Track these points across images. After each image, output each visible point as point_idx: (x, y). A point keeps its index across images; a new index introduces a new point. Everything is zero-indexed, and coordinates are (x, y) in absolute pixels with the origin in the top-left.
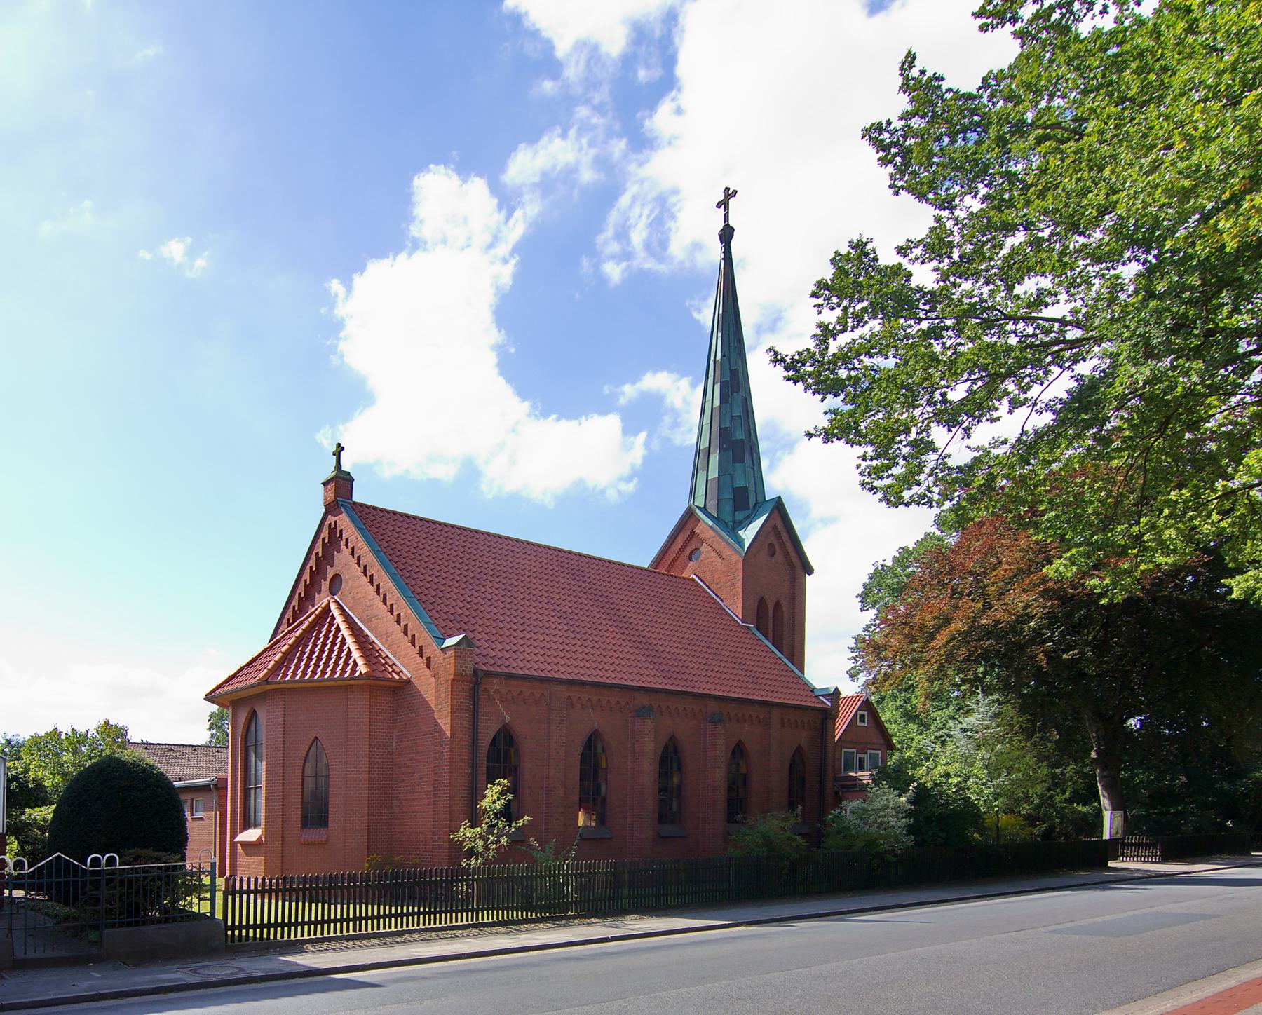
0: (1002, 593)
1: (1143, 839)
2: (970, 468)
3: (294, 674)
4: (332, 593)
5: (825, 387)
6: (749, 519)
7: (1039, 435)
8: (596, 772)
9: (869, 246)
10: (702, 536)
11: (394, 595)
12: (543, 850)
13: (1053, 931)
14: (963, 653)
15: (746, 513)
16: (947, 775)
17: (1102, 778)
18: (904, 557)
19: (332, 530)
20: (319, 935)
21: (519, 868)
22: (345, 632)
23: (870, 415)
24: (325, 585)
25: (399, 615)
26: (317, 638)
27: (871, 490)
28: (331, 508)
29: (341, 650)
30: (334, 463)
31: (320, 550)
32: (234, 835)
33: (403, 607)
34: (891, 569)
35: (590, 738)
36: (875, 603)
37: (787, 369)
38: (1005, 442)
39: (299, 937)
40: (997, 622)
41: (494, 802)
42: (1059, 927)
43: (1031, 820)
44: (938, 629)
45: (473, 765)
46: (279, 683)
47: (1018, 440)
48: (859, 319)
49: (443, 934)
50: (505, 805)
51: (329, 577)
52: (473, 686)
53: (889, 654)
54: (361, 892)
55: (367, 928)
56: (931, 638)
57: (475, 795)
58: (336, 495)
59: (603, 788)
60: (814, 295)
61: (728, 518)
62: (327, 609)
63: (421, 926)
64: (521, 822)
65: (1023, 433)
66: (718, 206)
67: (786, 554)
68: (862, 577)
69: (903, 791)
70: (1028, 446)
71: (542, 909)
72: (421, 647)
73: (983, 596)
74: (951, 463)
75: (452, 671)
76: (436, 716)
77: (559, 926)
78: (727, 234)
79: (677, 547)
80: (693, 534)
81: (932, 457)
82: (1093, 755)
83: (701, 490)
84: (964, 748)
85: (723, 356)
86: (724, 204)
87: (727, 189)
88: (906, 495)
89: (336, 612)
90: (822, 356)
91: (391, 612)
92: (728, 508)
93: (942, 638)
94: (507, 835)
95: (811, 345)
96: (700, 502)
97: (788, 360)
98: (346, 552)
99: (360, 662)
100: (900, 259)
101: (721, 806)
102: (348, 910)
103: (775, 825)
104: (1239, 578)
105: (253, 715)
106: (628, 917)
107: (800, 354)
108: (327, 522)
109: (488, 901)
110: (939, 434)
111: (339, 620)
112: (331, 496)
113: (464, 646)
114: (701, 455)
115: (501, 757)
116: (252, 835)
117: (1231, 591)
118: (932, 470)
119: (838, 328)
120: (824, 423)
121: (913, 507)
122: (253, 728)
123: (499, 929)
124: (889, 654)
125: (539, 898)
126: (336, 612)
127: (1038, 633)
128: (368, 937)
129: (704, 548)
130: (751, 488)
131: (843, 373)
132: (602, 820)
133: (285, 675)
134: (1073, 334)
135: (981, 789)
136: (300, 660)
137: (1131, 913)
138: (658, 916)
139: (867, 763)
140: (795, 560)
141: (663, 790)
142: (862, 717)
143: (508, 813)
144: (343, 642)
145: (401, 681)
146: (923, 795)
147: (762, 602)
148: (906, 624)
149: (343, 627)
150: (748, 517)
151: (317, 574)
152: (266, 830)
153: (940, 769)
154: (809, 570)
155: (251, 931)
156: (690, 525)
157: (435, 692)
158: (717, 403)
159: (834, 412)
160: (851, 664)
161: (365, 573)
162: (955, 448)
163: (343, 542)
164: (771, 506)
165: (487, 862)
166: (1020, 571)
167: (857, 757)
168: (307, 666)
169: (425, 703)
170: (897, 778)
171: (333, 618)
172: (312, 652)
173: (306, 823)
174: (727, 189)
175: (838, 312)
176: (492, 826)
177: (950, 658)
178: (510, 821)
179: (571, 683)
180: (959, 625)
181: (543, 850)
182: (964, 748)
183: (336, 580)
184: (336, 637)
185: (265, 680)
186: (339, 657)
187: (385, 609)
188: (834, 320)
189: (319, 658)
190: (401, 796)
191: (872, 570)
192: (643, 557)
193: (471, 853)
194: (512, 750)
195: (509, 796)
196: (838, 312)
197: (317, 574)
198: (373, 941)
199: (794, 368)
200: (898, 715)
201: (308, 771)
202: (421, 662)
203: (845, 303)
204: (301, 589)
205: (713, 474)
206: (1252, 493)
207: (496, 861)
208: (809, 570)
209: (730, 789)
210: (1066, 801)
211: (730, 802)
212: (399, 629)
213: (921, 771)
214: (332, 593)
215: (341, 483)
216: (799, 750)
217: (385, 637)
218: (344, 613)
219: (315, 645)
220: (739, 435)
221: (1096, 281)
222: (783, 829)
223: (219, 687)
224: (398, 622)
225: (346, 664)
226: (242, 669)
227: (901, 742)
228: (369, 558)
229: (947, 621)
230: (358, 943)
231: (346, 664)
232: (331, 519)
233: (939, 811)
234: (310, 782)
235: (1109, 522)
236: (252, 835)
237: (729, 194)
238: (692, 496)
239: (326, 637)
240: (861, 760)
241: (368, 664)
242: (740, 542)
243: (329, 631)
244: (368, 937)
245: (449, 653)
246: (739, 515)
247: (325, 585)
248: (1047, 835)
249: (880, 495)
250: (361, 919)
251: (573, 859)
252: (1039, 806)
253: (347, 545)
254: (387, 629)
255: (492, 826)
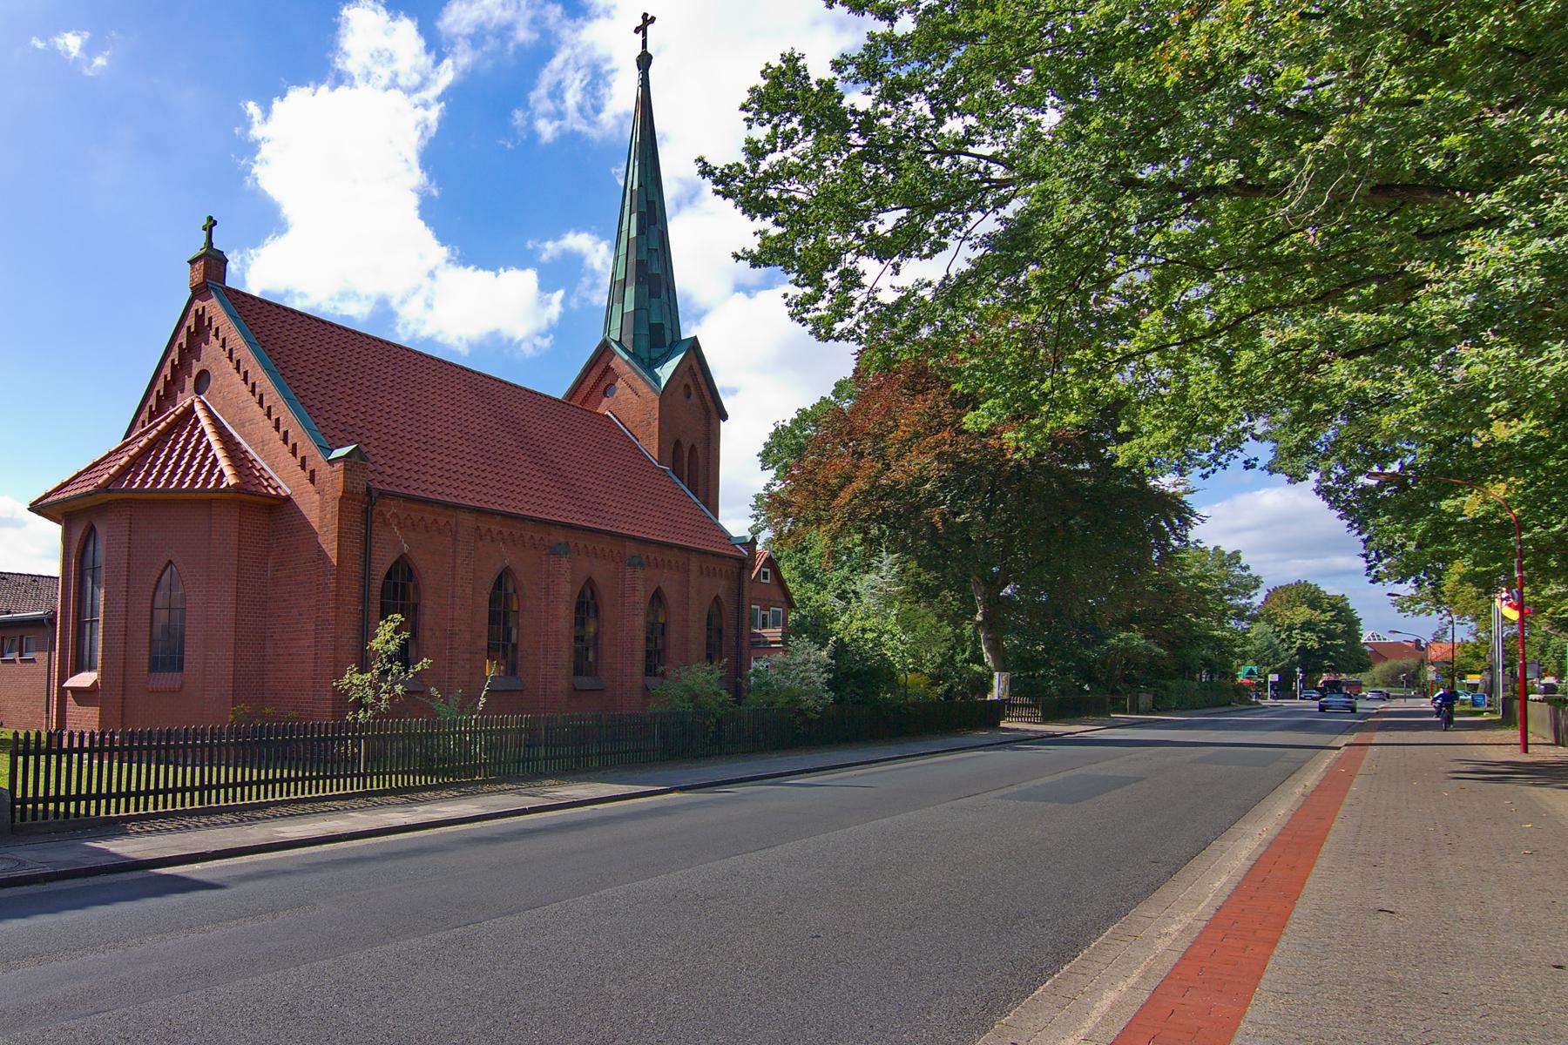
0: (900, 456)
1: (1025, 700)
2: (898, 307)
3: (144, 481)
4: (198, 390)
5: (754, 206)
6: (666, 358)
7: (963, 278)
8: (506, 614)
9: (800, 63)
10: (617, 371)
11: (273, 396)
12: (446, 702)
13: (1002, 797)
14: (866, 512)
15: (662, 351)
16: (864, 630)
17: (986, 640)
18: (803, 417)
19: (200, 318)
20: (151, 810)
21: (417, 723)
22: (211, 436)
23: (801, 249)
24: (189, 383)
25: (278, 420)
26: (176, 442)
27: (801, 321)
28: (199, 292)
29: (205, 457)
30: (204, 239)
31: (184, 341)
32: (63, 679)
33: (283, 411)
34: (791, 430)
35: (500, 576)
36: (775, 463)
37: (716, 182)
38: (929, 284)
39: (122, 813)
40: (897, 482)
41: (387, 642)
42: (1006, 791)
43: (935, 679)
44: (841, 488)
45: (365, 599)
46: (123, 491)
47: (942, 284)
48: (789, 139)
49: (319, 806)
50: (401, 646)
51: (195, 372)
52: (363, 504)
53: (794, 510)
54: (211, 752)
55: (217, 799)
56: (834, 495)
57: (367, 634)
58: (206, 274)
59: (514, 632)
60: (744, 108)
61: (645, 355)
62: (190, 410)
63: (292, 796)
64: (419, 667)
65: (947, 277)
66: (637, 31)
67: (702, 396)
68: (763, 436)
69: (823, 646)
70: (954, 291)
71: (446, 773)
72: (303, 459)
73: (882, 457)
74: (881, 297)
75: (340, 486)
76: (320, 540)
77: (465, 794)
78: (644, 61)
79: (591, 381)
80: (608, 369)
81: (859, 296)
82: (979, 618)
83: (616, 324)
84: (871, 605)
85: (640, 185)
86: (642, 29)
87: (646, 15)
88: (839, 327)
89: (201, 414)
90: (754, 171)
91: (269, 415)
92: (644, 344)
93: (845, 496)
94: (402, 682)
95: (741, 158)
96: (615, 335)
97: (717, 172)
98: (215, 343)
99: (228, 472)
100: (833, 75)
101: (640, 656)
102: (192, 775)
103: (700, 678)
104: (1126, 445)
105: (91, 532)
106: (546, 782)
107: (730, 168)
108: (194, 308)
109: (378, 762)
110: (869, 267)
111: (205, 423)
112: (199, 278)
113: (356, 459)
114: (618, 287)
115: (399, 590)
116: (85, 679)
117: (1114, 458)
118: (863, 304)
119: (768, 147)
120: (754, 245)
121: (842, 342)
122: (91, 548)
123: (391, 799)
124: (794, 510)
125: (442, 760)
126: (201, 414)
127: (932, 496)
128: (220, 811)
129: (620, 384)
130: (667, 325)
131: (773, 193)
132: (512, 670)
133: (132, 482)
134: (998, 172)
135: (895, 645)
136: (153, 466)
137: (1061, 776)
138: (579, 781)
139: (770, 619)
140: (710, 404)
141: (579, 639)
142: (765, 574)
143: (404, 656)
144: (209, 448)
145: (278, 497)
146: (841, 650)
147: (678, 443)
148: (809, 481)
149: (209, 430)
150: (663, 355)
151: (180, 369)
152: (103, 674)
153: (856, 625)
154: (725, 417)
155: (73, 804)
156: (605, 359)
157: (318, 508)
158: (633, 233)
159: (763, 233)
160: (752, 522)
161: (238, 369)
162: (883, 281)
163: (213, 332)
164: (687, 346)
165: (378, 715)
166: (917, 435)
167: (760, 613)
168: (161, 473)
169: (307, 524)
170: (816, 628)
171: (197, 420)
172: (168, 457)
173: (155, 666)
174: (646, 15)
175: (768, 129)
176: (385, 673)
177: (853, 516)
178: (407, 664)
179: (480, 511)
180: (860, 484)
181: (446, 702)
182: (871, 605)
183: (204, 376)
184: (199, 442)
185: (104, 488)
186: (201, 465)
187: (261, 412)
188: (763, 138)
189: (177, 465)
190: (277, 637)
191: (773, 429)
192: (557, 386)
193: (359, 704)
194: (411, 585)
195: (406, 635)
196: (768, 129)
197: (180, 369)
198: (226, 818)
199: (723, 181)
200: (795, 574)
201: (159, 602)
202: (303, 476)
203: (776, 120)
204: (160, 385)
205: (630, 307)
206: (1148, 357)
207: (388, 714)
208: (725, 417)
209: (648, 639)
210: (966, 661)
211: (649, 654)
212: (277, 436)
213: (837, 626)
214: (198, 390)
215: (211, 265)
216: (717, 598)
217: (261, 445)
218: (215, 421)
219: (172, 450)
220: (656, 269)
221: (1019, 125)
222: (708, 682)
223: (48, 495)
224: (277, 428)
225: (210, 473)
226: (79, 475)
227: (801, 601)
228: (244, 351)
229: (849, 479)
230: (204, 820)
231: (210, 473)
232: (198, 304)
233: (857, 667)
234: (162, 616)
235: (1025, 376)
236: (85, 679)
237: (647, 20)
238: (607, 330)
239: (187, 441)
240: (764, 617)
241: (238, 474)
242: (657, 379)
243: (191, 434)
244: (220, 811)
245: (339, 465)
246: (656, 353)
247: (189, 383)
248: (948, 693)
249: (810, 327)
250: (210, 787)
251: (481, 713)
252: (941, 665)
253: (217, 335)
254: (256, 430)
255: (385, 673)
